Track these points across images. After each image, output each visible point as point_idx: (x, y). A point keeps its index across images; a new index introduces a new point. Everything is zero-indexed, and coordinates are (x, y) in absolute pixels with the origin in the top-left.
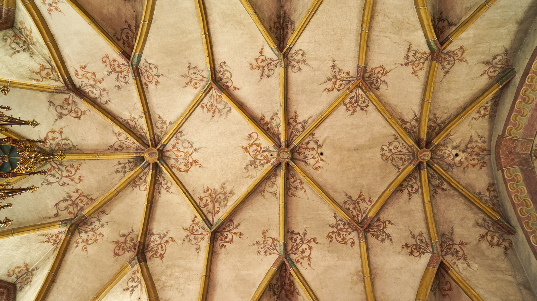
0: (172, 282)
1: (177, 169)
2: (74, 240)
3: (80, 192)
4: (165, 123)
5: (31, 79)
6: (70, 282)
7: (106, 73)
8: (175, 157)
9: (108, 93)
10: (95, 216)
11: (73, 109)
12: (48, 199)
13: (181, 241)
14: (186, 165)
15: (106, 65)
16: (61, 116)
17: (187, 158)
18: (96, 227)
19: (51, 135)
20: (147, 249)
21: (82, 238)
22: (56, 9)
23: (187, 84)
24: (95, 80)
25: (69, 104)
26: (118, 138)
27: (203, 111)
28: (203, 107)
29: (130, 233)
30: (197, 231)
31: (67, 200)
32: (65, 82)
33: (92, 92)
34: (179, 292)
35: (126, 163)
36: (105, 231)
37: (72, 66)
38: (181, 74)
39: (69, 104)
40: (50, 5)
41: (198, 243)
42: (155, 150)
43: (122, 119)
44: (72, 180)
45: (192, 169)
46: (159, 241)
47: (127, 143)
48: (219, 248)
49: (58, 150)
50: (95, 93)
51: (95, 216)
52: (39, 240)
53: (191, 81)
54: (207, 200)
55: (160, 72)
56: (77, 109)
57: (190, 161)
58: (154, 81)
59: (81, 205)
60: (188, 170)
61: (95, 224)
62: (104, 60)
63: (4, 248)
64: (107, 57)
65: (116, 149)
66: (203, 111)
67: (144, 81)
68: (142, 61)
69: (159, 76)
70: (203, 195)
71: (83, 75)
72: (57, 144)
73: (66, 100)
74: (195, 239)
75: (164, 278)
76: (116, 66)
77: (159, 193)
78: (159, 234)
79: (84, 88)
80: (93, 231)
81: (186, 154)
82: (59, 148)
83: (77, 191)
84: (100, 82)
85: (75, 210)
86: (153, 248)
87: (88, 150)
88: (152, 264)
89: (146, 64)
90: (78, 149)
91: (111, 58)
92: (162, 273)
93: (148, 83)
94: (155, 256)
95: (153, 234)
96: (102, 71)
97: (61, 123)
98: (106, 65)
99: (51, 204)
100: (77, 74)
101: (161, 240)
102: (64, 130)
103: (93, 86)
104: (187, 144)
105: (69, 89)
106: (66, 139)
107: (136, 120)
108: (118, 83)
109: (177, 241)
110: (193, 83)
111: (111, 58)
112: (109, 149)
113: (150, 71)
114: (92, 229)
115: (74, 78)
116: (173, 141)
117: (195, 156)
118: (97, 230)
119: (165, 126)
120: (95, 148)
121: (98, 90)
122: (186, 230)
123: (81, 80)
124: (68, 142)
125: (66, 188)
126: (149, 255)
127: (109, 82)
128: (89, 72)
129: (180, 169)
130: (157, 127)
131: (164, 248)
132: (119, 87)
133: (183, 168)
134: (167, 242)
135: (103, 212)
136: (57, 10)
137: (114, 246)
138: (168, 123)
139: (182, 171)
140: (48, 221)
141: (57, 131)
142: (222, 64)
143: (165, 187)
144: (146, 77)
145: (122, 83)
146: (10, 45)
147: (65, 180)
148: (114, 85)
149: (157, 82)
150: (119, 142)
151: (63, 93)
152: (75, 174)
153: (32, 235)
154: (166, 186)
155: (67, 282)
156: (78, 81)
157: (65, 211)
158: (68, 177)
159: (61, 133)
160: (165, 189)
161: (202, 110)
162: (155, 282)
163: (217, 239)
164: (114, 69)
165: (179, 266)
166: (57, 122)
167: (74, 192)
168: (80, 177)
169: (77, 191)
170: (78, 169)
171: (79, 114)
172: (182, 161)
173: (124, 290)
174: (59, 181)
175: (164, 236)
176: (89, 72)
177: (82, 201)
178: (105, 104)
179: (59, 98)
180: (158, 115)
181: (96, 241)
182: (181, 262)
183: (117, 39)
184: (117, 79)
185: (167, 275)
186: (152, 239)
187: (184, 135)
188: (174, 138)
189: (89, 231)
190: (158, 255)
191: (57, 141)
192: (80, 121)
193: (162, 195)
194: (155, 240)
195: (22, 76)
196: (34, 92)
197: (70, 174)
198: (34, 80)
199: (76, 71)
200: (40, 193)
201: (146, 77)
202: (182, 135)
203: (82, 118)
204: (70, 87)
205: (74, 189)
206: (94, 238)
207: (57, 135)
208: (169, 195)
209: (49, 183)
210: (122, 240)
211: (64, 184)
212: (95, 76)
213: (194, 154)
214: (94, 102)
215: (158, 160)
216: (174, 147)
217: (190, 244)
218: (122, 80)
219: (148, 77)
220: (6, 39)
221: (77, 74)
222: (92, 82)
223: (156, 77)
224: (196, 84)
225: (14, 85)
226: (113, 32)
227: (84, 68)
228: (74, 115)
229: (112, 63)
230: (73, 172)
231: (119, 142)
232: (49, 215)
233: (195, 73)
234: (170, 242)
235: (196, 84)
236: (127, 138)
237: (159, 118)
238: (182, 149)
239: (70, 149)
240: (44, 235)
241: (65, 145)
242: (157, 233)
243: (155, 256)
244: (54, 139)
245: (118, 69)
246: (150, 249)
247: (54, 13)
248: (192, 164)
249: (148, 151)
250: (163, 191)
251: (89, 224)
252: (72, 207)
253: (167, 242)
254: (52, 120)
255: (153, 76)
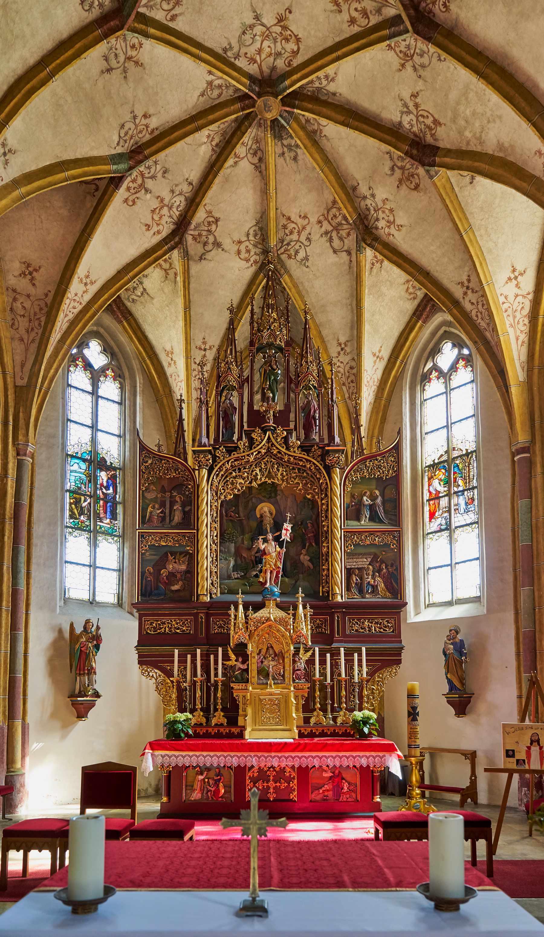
0: (477, 124)
1: (294, 57)
2: (384, 238)
3: (321, 218)
4: (210, 83)
5: (175, 282)
6: (434, 255)
7: (148, 196)
8: (272, 59)
9: (177, 185)
10: (358, 202)
11: (206, 229)
12: (326, 261)
13: (421, 82)
14: (287, 40)
15: (138, 198)
16: (218, 244)
17: (274, 35)
18: (374, 204)
19: (244, 255)
20: (420, 138)
21: (384, 227)
22: (87, 277)
23: (137, 63)
24: (162, 208)
25: (200, 235)
26: (243, 158)
27: (181, 14)
28: (173, 18)
29: (391, 159)
30: (408, 47)
31: (331, 237)
32: (172, 249)
33: (179, 206)
34: (494, 121)
35: (283, 144)
36: (381, 194)
37: (149, 240)
38: (123, 81)
39: (200, 235)
40: (86, 284)
41: (430, 54)
42: (260, 102)
43: (212, 155)
44: (304, 228)
45: (293, 27)
46: (412, 116)
47: (250, 143)
48: (446, 15)
49: (263, 244)
50: (180, 202)
51: (358, 202)
52: (377, 273)
53: (129, 58)
54: (356, 9)
55: (129, 117)
56: (206, 224)
57: (278, 29)
58: (144, 122)
59: (340, 218)
60: (296, 36)
61: (369, 205)
62: (131, 203)
63: (378, 309)
64: (126, 201)
65: (260, 160)
66: (181, 14)
67: (148, 137)
68: (119, 150)
69: (135, 117)
70: (345, 17)
71: (158, 225)
72: (255, 246)
73: (195, 239)
74: (422, 56)
75: (468, 134)
76: (135, 185)
77: (334, 94)
78: (402, 113)
79: (175, 218)
80: (378, 210)
81: (266, 36)
82: (260, 244)
83: (320, 222)
84: (162, 201)
85: (345, 227)
86: (421, 130)
87: (262, 204)
88: (443, 140)
89: (122, 143)
90: (261, 217)
91: (127, 195)
92: (460, 133)
93: (149, 129)
94: (433, 132)
95: (400, 123)
96: (148, 202)
97: (227, 243)
98: (138, 198)
99: (333, 258)
100: (159, 232)
101: (412, 113)
102: (236, 239)
103: (170, 208)
104: (247, 37)
105: (180, 242)
106: (248, 235)
107: (211, 133)
108: (159, 175)
109: (418, 89)
110: (134, 53)
111: (127, 195)
112: (260, 172)
113: (130, 132)
114: (375, 210)
115: (164, 234)
116: (242, 63)
117: (269, 19)
118: (377, 206)
119: (217, 82)
120: (259, 193)
121: (174, 199)
122: (403, 65)
123: (165, 225)
124: (251, 232)
125: (315, 237)
126: (429, 139)
127: (160, 187)
128: (153, 218)
129: (293, 52)
130: (220, 95)
131: (425, 114)
132: (165, 172)
133: (291, 46)
134: (416, 106)
135: (354, 189)
136: (88, 276)
137: (404, 187)
138: (211, 78)
139: (299, 49)
140: (354, 263)
141: (237, 247)
142: (87, 8)
143: (324, 82)
144: (140, 135)
145: (158, 169)
146: (140, 297)
147: (303, 238)
148: (163, 179)
149: (145, 116)
150: (249, 155)
151: (186, 247)
152: (296, 223)
153: (367, 280)
154: (323, 80)
155: (433, 259)
156: (166, 229)
157: (346, 240)
158: (299, 233)
159: (240, 242)
160: (329, 83)
161: (180, 18)
162: (470, 148)
163: (431, 11)
164: (140, 186)
165: (458, 103)
166: (226, 249)
167: (321, 227)
168: (300, 216)
169: (320, 222)
170: (289, 219)
171: (211, 219)
172: (278, 44)
173: (471, 183)
174: (305, 246)
175: (407, 107)
176: (153, 218)
177: (335, 216)
178: (192, 184)
179: (194, 248)
180: (198, 100)
181: (391, 210)
182: (453, 95)
183: (97, 190)
184: (153, 177)
185: (465, 128)
186: (407, 126)
187: (230, 44)
188: (237, 62)
189: (377, 216)
190: (433, 126)
191: (251, 247)
192: (222, 217)
193: (339, 91)
194: (409, 123)
195: (175, 291)
196: (192, 280)
197: (296, 231)
198: (176, 278)
199: (154, 234)
200: (318, 270)
201: (140, 135)
202: (231, 48)
203: (216, 215)
204: (177, 239)
205: (316, 226)
206: (387, 211)
207: (243, 248)
208: (340, 78)
209: (306, 258)
210: (398, 173)
211: (308, 239)
212: (155, 209)
213: (264, 21)
214: (194, 201)
215: (276, 97)
216: (252, 60)
217: (428, 69)
218: (153, 170)
219: (141, 132)
220: (133, 300)
221: (159, 232)
222: (165, 211)
223: (137, 121)
224: (133, 47)
225: (187, 303)
226: (88, 198)
227: (149, 226)
228: (213, 227)
229: (132, 191)
230: (293, 225)
231: (249, 155)
232: (347, 262)
233: (116, 55)
234: (418, 100)
235: (133, 47)
236: (243, 144)
237: (202, 95)
238: (257, 45)
239: (261, 229)
240: (372, 268)
241: (255, 235)
242: (399, 115)
243: (433, 132)
244: (248, 251)
245: (139, 181)
246: (421, 135)
247: (93, 277)
248: (285, 28)
249: (261, 113)
250: (332, 87)
251: (368, 213)
252: (341, 232)
253: (416, 106)
254: (224, 255)
255: (136, 126)
